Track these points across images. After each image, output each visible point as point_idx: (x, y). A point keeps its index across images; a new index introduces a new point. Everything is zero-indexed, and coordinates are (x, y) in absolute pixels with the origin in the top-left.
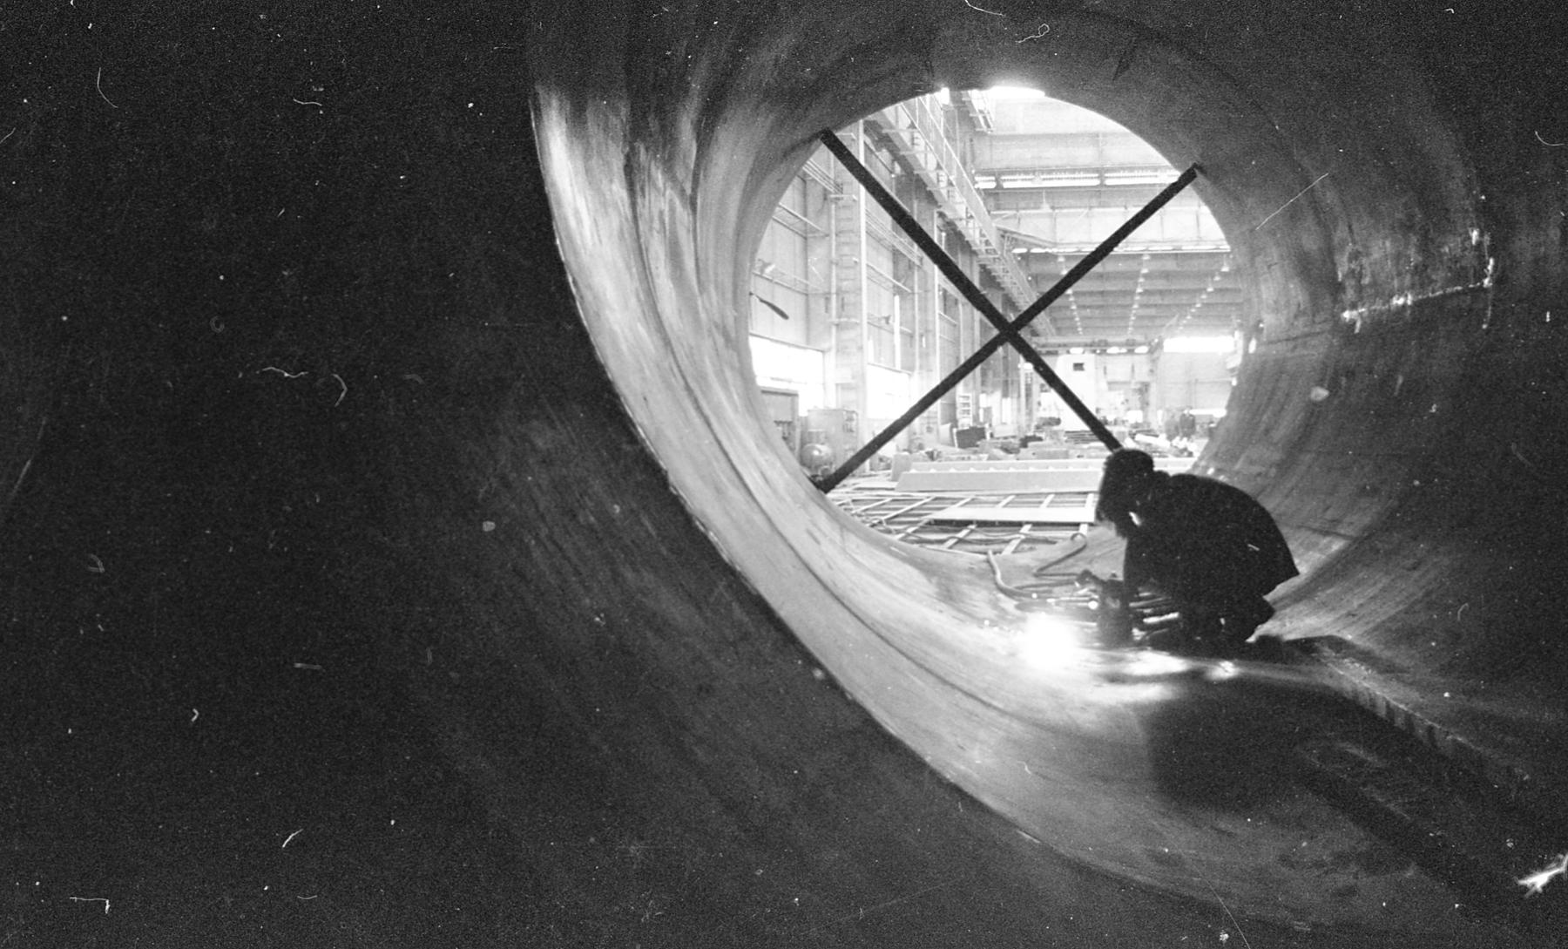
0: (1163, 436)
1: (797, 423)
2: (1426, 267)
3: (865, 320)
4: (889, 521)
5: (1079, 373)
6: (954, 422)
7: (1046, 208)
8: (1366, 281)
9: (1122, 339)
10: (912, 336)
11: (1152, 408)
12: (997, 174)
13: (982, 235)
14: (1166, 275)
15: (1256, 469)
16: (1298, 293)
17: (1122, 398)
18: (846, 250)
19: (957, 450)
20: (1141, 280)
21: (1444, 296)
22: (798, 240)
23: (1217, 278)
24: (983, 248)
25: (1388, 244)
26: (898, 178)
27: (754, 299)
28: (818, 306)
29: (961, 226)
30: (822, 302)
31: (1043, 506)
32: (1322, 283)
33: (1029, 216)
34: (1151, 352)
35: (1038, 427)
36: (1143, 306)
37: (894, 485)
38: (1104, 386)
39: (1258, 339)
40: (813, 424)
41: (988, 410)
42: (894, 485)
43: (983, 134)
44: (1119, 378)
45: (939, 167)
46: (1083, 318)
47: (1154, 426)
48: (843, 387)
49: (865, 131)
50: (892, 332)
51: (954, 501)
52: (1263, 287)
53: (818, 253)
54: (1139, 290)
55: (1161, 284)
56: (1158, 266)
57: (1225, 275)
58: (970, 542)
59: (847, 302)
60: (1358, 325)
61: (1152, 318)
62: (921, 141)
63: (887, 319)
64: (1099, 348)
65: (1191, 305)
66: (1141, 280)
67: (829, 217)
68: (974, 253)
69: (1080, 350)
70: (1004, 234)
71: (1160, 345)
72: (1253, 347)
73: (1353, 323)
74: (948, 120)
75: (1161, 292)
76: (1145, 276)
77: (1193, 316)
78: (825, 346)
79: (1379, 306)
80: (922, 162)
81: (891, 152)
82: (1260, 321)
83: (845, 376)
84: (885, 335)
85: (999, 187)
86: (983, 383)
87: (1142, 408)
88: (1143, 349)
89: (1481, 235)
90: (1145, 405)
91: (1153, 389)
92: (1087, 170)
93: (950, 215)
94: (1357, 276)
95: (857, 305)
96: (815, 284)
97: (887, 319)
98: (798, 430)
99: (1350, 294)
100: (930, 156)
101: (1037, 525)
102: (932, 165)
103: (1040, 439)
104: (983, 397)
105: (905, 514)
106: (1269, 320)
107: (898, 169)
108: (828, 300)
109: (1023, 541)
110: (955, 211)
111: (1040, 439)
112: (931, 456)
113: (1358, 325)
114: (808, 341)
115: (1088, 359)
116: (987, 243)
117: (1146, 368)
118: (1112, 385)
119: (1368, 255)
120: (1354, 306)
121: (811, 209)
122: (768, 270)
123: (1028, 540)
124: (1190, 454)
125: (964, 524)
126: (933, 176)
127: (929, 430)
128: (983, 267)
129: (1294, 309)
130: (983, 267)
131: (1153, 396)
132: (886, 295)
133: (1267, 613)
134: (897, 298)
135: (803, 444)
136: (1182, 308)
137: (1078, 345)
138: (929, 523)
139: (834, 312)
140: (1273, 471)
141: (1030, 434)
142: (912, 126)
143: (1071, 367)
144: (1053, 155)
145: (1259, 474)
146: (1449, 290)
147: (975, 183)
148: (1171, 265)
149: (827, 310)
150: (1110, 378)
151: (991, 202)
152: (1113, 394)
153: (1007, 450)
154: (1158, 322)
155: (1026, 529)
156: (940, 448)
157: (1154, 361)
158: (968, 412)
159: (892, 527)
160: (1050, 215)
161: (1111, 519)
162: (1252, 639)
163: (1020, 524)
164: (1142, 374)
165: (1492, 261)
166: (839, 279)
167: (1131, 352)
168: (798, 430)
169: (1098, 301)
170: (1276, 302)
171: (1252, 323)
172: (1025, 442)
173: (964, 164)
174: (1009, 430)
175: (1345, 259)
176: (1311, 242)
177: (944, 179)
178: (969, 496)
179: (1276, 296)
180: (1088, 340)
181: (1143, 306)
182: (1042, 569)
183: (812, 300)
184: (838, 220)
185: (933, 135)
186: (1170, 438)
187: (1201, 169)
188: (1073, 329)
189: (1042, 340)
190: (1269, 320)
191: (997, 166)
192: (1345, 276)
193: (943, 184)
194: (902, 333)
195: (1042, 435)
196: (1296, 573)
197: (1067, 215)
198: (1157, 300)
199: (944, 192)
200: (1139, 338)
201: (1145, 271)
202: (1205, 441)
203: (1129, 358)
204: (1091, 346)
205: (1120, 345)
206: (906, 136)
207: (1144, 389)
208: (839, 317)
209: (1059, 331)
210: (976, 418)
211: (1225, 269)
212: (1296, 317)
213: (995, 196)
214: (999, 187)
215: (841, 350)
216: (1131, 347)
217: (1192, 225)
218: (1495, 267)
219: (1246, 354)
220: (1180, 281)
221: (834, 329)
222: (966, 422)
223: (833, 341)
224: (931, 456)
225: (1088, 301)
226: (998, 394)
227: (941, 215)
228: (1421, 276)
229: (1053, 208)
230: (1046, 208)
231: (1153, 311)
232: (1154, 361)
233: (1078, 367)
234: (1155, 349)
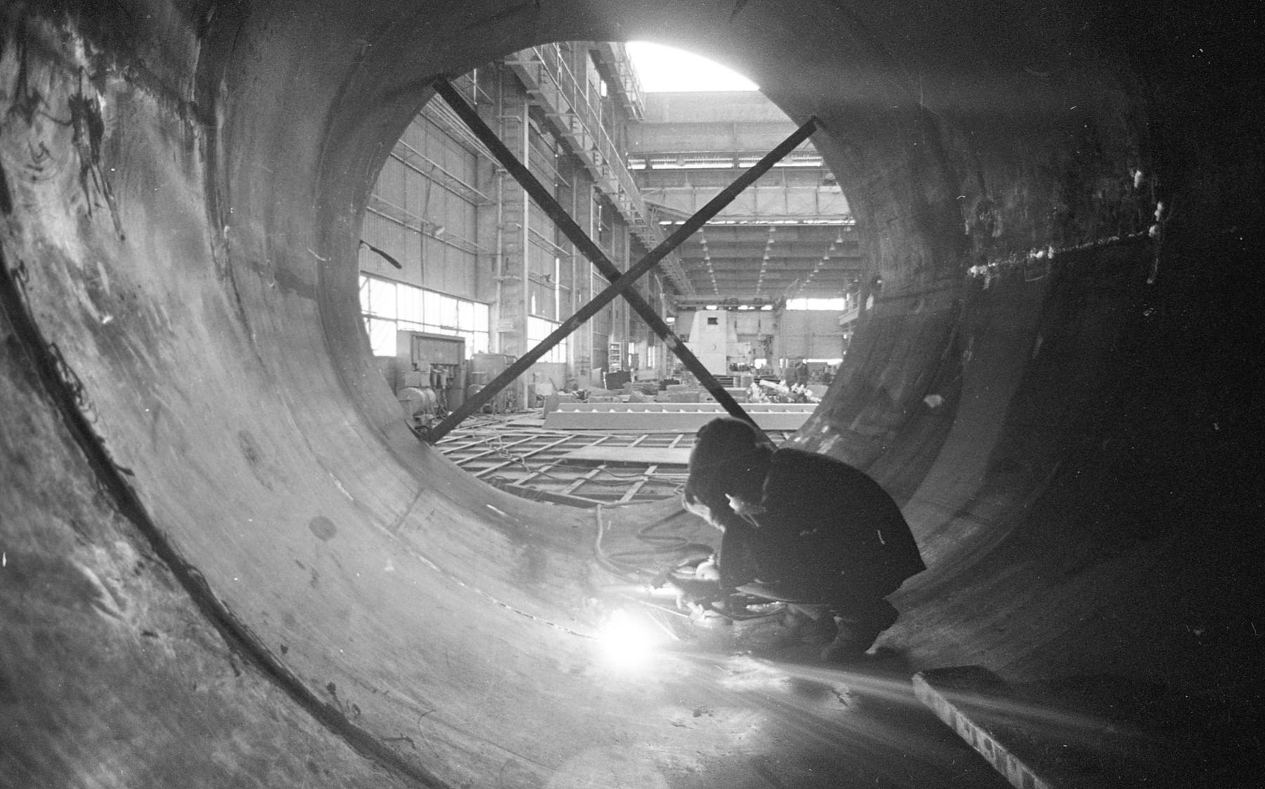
0: (783, 382)
1: (463, 367)
2: (1072, 216)
3: (526, 277)
4: (528, 459)
5: (713, 326)
6: (605, 366)
7: (688, 187)
8: (997, 233)
9: (751, 298)
10: (569, 293)
11: (775, 356)
12: (648, 157)
13: (632, 208)
14: (790, 245)
15: (873, 431)
16: (920, 251)
17: (749, 348)
18: (511, 217)
19: (606, 390)
20: (768, 249)
21: (1096, 248)
22: (469, 208)
23: (832, 249)
24: (633, 219)
25: (1025, 192)
26: (560, 157)
27: (365, 249)
28: (485, 264)
29: (614, 199)
30: (489, 263)
31: (672, 446)
32: (945, 235)
33: (673, 192)
34: (774, 309)
35: (677, 372)
36: (768, 271)
37: (542, 422)
38: (734, 337)
39: (875, 296)
40: (477, 367)
41: (635, 357)
42: (542, 422)
43: (636, 123)
44: (748, 331)
45: (595, 148)
46: (717, 281)
47: (777, 373)
48: (505, 335)
49: (530, 115)
50: (553, 289)
51: (592, 439)
52: (882, 242)
53: (487, 219)
54: (766, 257)
55: (785, 253)
56: (782, 237)
57: (839, 246)
58: (597, 483)
59: (510, 260)
60: (988, 281)
61: (777, 281)
62: (579, 126)
63: (548, 277)
64: (731, 306)
65: (811, 271)
66: (768, 249)
67: (497, 190)
68: (626, 223)
69: (714, 307)
70: (651, 208)
71: (783, 304)
72: (870, 303)
73: (981, 278)
74: (605, 110)
75: (785, 259)
76: (771, 245)
77: (813, 280)
78: (491, 299)
79: (1012, 261)
80: (580, 143)
81: (553, 133)
82: (879, 278)
83: (508, 325)
84: (548, 291)
85: (649, 167)
86: (632, 334)
87: (766, 357)
88: (769, 307)
89: (1146, 175)
90: (768, 355)
91: (776, 342)
92: (722, 154)
93: (604, 189)
94: (985, 229)
95: (520, 265)
96: (483, 245)
97: (548, 277)
98: (463, 372)
99: (978, 248)
100: (587, 138)
101: (662, 466)
102: (589, 146)
103: (677, 383)
104: (631, 346)
105: (546, 452)
106: (887, 276)
107: (560, 150)
108: (494, 260)
109: (646, 484)
110: (607, 185)
111: (677, 383)
112: (582, 397)
113: (988, 281)
114: (476, 295)
115: (722, 315)
116: (637, 215)
117: (770, 323)
118: (741, 337)
119: (1001, 205)
120: (982, 261)
121: (481, 181)
122: (439, 232)
123: (652, 482)
124: (806, 400)
125: (593, 464)
126: (590, 155)
127: (583, 373)
128: (633, 235)
129: (915, 264)
130: (633, 235)
131: (776, 346)
132: (548, 257)
133: (891, 618)
134: (558, 260)
135: (468, 383)
136: (803, 273)
137: (713, 303)
138: (563, 463)
139: (499, 270)
140: (892, 434)
141: (668, 378)
142: (571, 111)
143: (706, 321)
144: (696, 141)
145: (874, 437)
146: (1101, 241)
147: (627, 164)
148: (794, 237)
149: (494, 268)
150: (740, 331)
151: (642, 181)
152: (741, 344)
153: (647, 391)
154: (782, 285)
155: (650, 471)
156: (591, 389)
157: (777, 317)
158: (617, 358)
159: (528, 465)
160: (691, 192)
161: (704, 502)
162: (871, 651)
163: (646, 465)
164: (767, 328)
165: (1160, 206)
166: (505, 242)
167: (758, 309)
168: (463, 372)
169: (730, 266)
170: (896, 259)
171: (870, 278)
172: (664, 385)
173: (618, 147)
174: (651, 375)
175: (974, 209)
176: (933, 194)
177: (599, 158)
178: (607, 435)
179: (896, 254)
180: (722, 299)
181: (768, 271)
182: (649, 529)
183: (480, 258)
184: (504, 192)
185: (589, 120)
186: (789, 384)
187: (820, 123)
188: (710, 290)
189: (683, 298)
190: (887, 276)
191: (645, 149)
192: (972, 229)
193: (598, 163)
194: (561, 289)
195: (679, 379)
196: (921, 566)
197: (703, 192)
198: (781, 265)
199: (599, 170)
200: (765, 297)
201: (771, 241)
202: (824, 389)
203: (755, 315)
204: (724, 304)
205: (749, 303)
206: (565, 120)
207: (768, 341)
208: (504, 273)
209: (699, 291)
210: (624, 363)
211: (840, 241)
212: (917, 272)
213: (647, 177)
214: (649, 167)
215: (505, 303)
216: (758, 304)
217: (812, 199)
218: (1163, 213)
219: (863, 312)
220: (803, 255)
221: (499, 286)
222: (615, 366)
223: (498, 296)
224: (582, 397)
225: (723, 266)
226: (644, 344)
227: (598, 190)
228: (1066, 227)
229: (694, 186)
230: (688, 187)
231: (778, 276)
232: (777, 317)
233: (712, 321)
234: (779, 306)
